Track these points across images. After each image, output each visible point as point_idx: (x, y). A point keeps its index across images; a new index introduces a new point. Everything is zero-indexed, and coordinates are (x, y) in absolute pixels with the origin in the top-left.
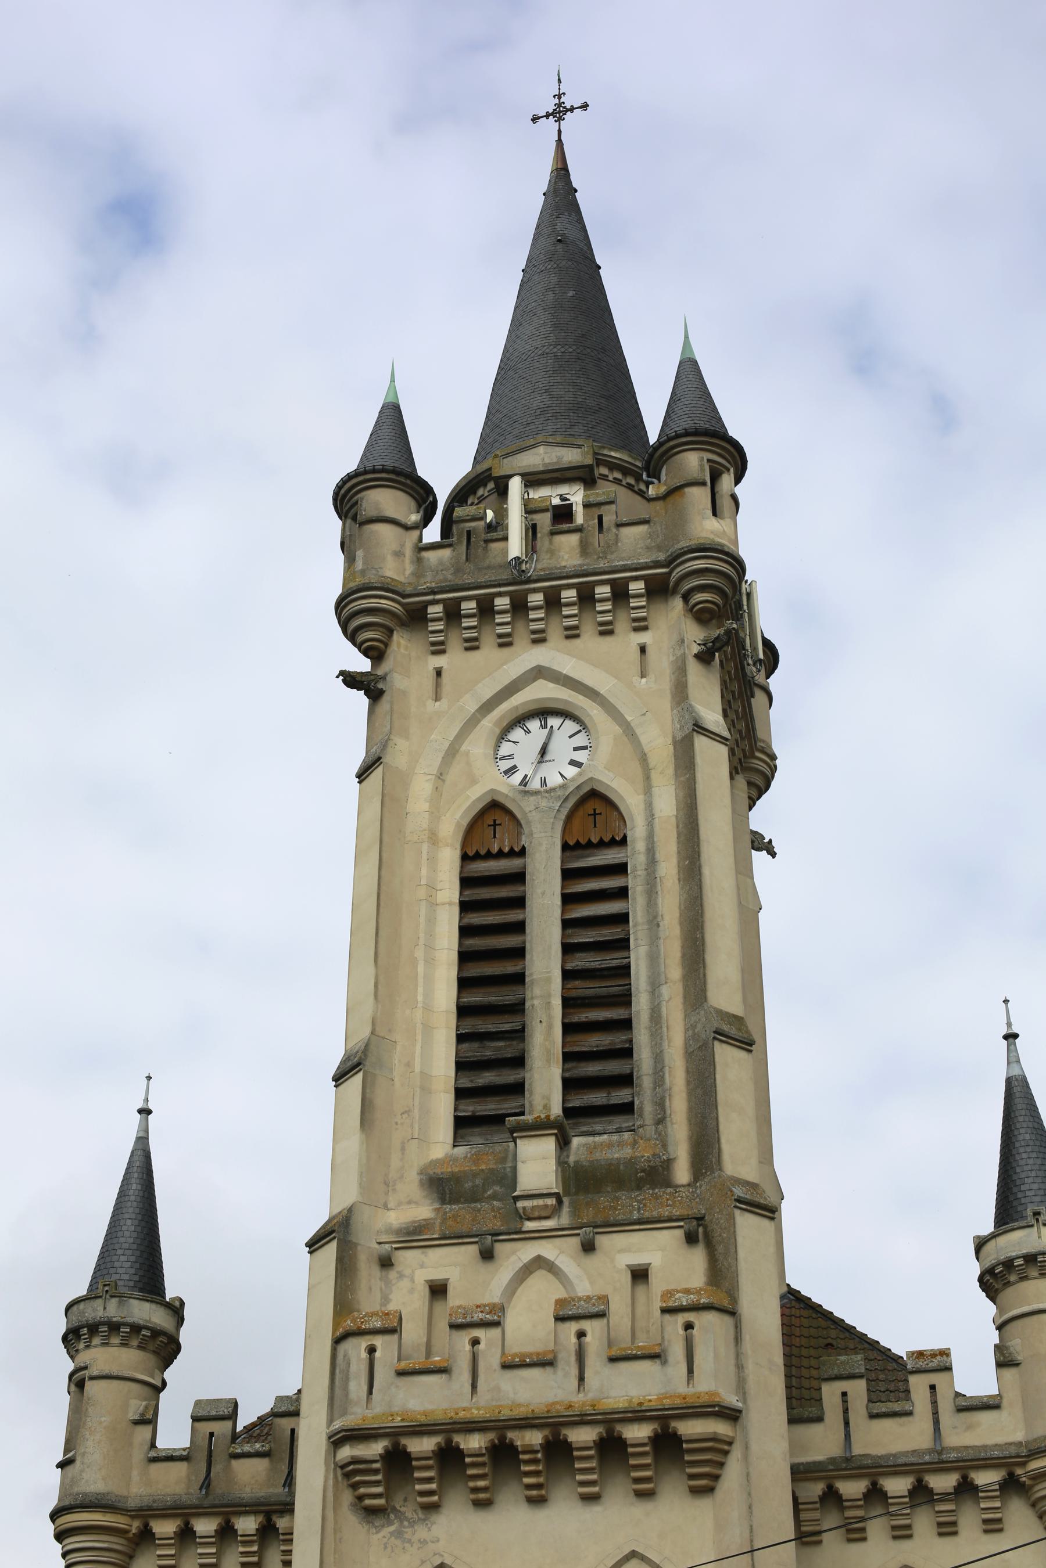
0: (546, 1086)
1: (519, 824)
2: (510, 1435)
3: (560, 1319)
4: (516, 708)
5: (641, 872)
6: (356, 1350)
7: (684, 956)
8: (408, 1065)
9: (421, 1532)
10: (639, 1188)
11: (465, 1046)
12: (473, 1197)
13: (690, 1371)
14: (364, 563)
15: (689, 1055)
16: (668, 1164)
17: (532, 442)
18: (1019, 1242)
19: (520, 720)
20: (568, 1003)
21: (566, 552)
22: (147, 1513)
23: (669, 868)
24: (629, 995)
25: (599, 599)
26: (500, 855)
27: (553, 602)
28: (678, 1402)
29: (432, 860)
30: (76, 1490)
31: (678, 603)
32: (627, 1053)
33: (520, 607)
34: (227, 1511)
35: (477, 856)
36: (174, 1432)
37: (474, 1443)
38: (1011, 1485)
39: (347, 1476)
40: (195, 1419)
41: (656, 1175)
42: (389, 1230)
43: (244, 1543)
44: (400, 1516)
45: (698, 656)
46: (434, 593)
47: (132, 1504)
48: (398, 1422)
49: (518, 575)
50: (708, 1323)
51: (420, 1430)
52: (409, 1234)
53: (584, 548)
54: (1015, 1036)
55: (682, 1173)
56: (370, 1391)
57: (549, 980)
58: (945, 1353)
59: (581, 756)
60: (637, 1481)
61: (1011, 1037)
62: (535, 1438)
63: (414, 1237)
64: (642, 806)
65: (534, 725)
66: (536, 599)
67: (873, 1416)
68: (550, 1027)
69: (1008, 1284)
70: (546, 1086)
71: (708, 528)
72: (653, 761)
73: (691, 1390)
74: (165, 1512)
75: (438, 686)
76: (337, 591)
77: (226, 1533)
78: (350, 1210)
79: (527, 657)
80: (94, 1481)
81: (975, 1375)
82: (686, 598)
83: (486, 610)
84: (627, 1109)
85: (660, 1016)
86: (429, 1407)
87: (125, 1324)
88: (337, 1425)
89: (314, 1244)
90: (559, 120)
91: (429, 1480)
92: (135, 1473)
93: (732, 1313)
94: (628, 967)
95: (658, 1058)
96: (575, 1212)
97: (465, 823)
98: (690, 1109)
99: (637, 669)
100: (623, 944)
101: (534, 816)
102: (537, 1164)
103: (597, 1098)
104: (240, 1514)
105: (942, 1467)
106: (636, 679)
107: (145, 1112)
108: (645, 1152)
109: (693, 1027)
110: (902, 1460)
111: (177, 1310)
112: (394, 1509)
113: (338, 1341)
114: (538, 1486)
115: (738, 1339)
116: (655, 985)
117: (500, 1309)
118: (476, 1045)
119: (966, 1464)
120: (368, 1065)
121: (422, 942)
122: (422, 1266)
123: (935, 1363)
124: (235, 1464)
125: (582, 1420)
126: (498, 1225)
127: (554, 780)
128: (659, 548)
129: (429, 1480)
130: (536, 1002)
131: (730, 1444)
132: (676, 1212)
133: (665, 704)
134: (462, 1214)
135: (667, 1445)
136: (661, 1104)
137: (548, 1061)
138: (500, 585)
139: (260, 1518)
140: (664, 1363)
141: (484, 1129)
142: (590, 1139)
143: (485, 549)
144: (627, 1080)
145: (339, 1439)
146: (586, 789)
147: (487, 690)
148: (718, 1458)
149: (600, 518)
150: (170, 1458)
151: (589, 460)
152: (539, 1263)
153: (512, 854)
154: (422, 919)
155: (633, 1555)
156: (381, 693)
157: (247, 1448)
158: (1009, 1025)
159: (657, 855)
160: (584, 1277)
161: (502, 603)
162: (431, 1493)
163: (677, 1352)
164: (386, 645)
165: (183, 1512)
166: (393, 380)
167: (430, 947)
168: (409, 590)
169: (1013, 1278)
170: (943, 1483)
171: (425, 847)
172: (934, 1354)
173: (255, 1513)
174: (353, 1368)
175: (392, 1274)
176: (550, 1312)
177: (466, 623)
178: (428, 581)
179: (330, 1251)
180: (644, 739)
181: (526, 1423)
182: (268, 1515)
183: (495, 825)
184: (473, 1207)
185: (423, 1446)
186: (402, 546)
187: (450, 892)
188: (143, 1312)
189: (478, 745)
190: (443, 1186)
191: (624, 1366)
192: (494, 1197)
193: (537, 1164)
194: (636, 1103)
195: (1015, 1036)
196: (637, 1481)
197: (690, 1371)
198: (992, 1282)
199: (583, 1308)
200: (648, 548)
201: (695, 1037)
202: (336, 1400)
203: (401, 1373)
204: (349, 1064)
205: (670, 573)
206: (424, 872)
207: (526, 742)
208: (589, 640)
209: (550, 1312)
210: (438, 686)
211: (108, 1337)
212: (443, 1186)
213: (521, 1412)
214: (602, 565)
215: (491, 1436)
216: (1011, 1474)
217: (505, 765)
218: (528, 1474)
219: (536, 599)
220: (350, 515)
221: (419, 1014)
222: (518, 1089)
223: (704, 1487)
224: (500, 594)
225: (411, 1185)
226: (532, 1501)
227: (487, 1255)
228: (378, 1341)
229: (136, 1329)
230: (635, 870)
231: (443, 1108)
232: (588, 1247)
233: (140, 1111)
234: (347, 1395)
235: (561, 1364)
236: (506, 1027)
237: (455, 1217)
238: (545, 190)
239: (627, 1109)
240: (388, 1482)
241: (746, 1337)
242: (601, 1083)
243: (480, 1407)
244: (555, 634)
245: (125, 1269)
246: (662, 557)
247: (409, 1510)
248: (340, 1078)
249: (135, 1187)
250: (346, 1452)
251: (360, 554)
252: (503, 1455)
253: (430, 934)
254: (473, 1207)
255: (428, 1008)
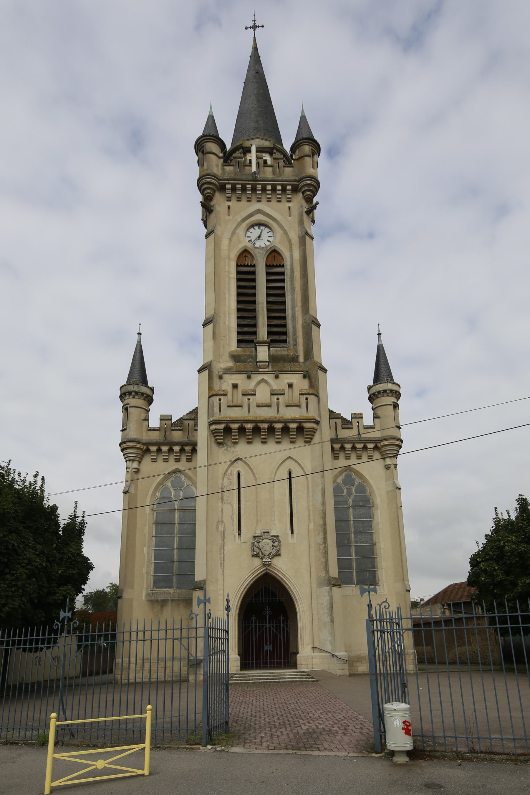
0: (262, 332)
1: (253, 257)
2: (259, 424)
3: (272, 394)
4: (252, 221)
5: (289, 275)
6: (216, 399)
7: (302, 299)
8: (225, 323)
9: (233, 449)
10: (290, 362)
11: (239, 320)
12: (244, 361)
13: (307, 410)
14: (207, 166)
15: (303, 327)
16: (298, 357)
17: (255, 137)
18: (381, 387)
19: (252, 226)
20: (268, 310)
21: (268, 173)
22: (149, 444)
23: (297, 274)
24: (285, 310)
25: (276, 190)
26: (247, 266)
27: (264, 189)
28: (304, 418)
29: (229, 264)
30: (127, 437)
31: (300, 195)
32: (285, 326)
33: (254, 189)
34: (171, 444)
35: (241, 266)
36: (154, 422)
37: (249, 426)
38: (376, 448)
39: (213, 433)
40: (161, 420)
41: (294, 359)
42: (221, 369)
43: (176, 453)
44: (227, 445)
45: (306, 212)
46: (228, 180)
47: (144, 441)
48: (228, 419)
49: (254, 178)
50: (312, 398)
51: (234, 422)
52: (227, 370)
53: (274, 172)
54: (381, 334)
55: (301, 359)
56: (220, 411)
57: (263, 303)
58: (361, 414)
59: (270, 239)
60: (291, 438)
61: (379, 334)
62: (266, 426)
63: (228, 371)
64: (289, 256)
65: (257, 228)
66: (259, 187)
67: (343, 428)
68: (264, 316)
69: (378, 397)
70: (262, 332)
71: (310, 171)
72: (293, 242)
73: (307, 415)
74: (153, 444)
75: (229, 212)
76: (197, 177)
77: (171, 450)
78: (211, 362)
79: (255, 206)
80: (132, 434)
81: (368, 420)
82: (303, 193)
83: (244, 189)
84: (285, 341)
85: (295, 316)
86: (237, 416)
87: (140, 392)
88: (211, 419)
89: (200, 371)
90: (254, 30)
91: (236, 436)
92: (144, 434)
93: (317, 396)
94: (285, 302)
95: (295, 328)
96: (273, 367)
97: (238, 255)
98: (304, 342)
99: (288, 214)
100: (284, 295)
101: (258, 255)
102: (263, 353)
103: (277, 338)
104: (174, 445)
105: (360, 442)
106: (288, 217)
107: (139, 334)
108: (291, 353)
109: (305, 319)
110: (126, 524)
111: (152, 389)
112: (225, 443)
113: (209, 397)
114: (265, 439)
115: (319, 403)
116: (293, 308)
117: (254, 391)
118: (242, 320)
119: (365, 442)
120: (214, 321)
121: (227, 288)
122: (231, 379)
123: (359, 416)
124: (172, 432)
125: (279, 421)
126: (252, 369)
127: (263, 245)
128: (296, 176)
129: (236, 436)
130: (260, 309)
131: (316, 430)
132: (301, 369)
133: (296, 225)
134: (242, 366)
135: (300, 430)
136: (295, 340)
137: (263, 326)
138: (248, 181)
139: (180, 447)
140: (300, 408)
141: (245, 344)
142: (275, 349)
143: (244, 168)
144: (285, 333)
145: (211, 424)
146: (273, 249)
147: (245, 214)
148: (313, 433)
149: (278, 163)
150: (154, 430)
151: (272, 146)
152: (263, 380)
153: (251, 266)
154: (227, 282)
155: (289, 457)
156: (212, 211)
157: (176, 428)
158: (379, 331)
159: (294, 270)
160: (276, 385)
161: (249, 187)
162: (236, 439)
163: (304, 405)
164: (213, 196)
165: (159, 444)
166: (211, 108)
167: (229, 290)
168: (221, 178)
169: (379, 396)
170: (359, 446)
171: (227, 260)
172: (358, 414)
173: (179, 445)
174: (215, 404)
175: (222, 381)
176: (265, 394)
177: (238, 192)
178: (226, 176)
179: (206, 373)
180: (290, 235)
181: (263, 421)
182: (182, 446)
183: (246, 257)
184: (244, 364)
185: (235, 426)
186: (218, 163)
187: (234, 275)
188: (143, 389)
189: (241, 231)
190: (235, 358)
191: (289, 408)
192: (250, 362)
193: (263, 353)
194: (288, 340)
195: (381, 334)
196: (291, 438)
197: (307, 410)
198: (371, 399)
199: (279, 392)
200: (293, 175)
201: (305, 322)
202: (210, 412)
203: (229, 406)
204: (208, 321)
205: (299, 184)
206: (227, 267)
207: (255, 232)
208: (274, 203)
209: (265, 394)
210: (229, 212)
211: (135, 396)
212: (235, 358)
213: (261, 419)
214: (279, 178)
215: (254, 424)
216: (376, 445)
217: (249, 239)
218: (263, 435)
219: (259, 187)
220: (201, 150)
221: (227, 309)
222: (255, 333)
223: (308, 441)
224: (248, 184)
225: (226, 357)
226: (263, 442)
227: (249, 377)
228: (222, 397)
229: (143, 394)
230: (287, 274)
231: (234, 337)
232: (277, 377)
233: (138, 334)
234: (213, 411)
235: (273, 406)
236: (251, 316)
237: (239, 366)
238: (250, 55)
239: (285, 341)
240: (224, 436)
241: (321, 403)
242: (278, 334)
243: (251, 416)
244: (264, 199)
245: (137, 376)
246: (297, 179)
247: (229, 443)
248: (204, 325)
249: (138, 355)
250: (213, 427)
251: (205, 163)
252: (256, 430)
253: (229, 286)
254: (244, 364)
255: (229, 308)
